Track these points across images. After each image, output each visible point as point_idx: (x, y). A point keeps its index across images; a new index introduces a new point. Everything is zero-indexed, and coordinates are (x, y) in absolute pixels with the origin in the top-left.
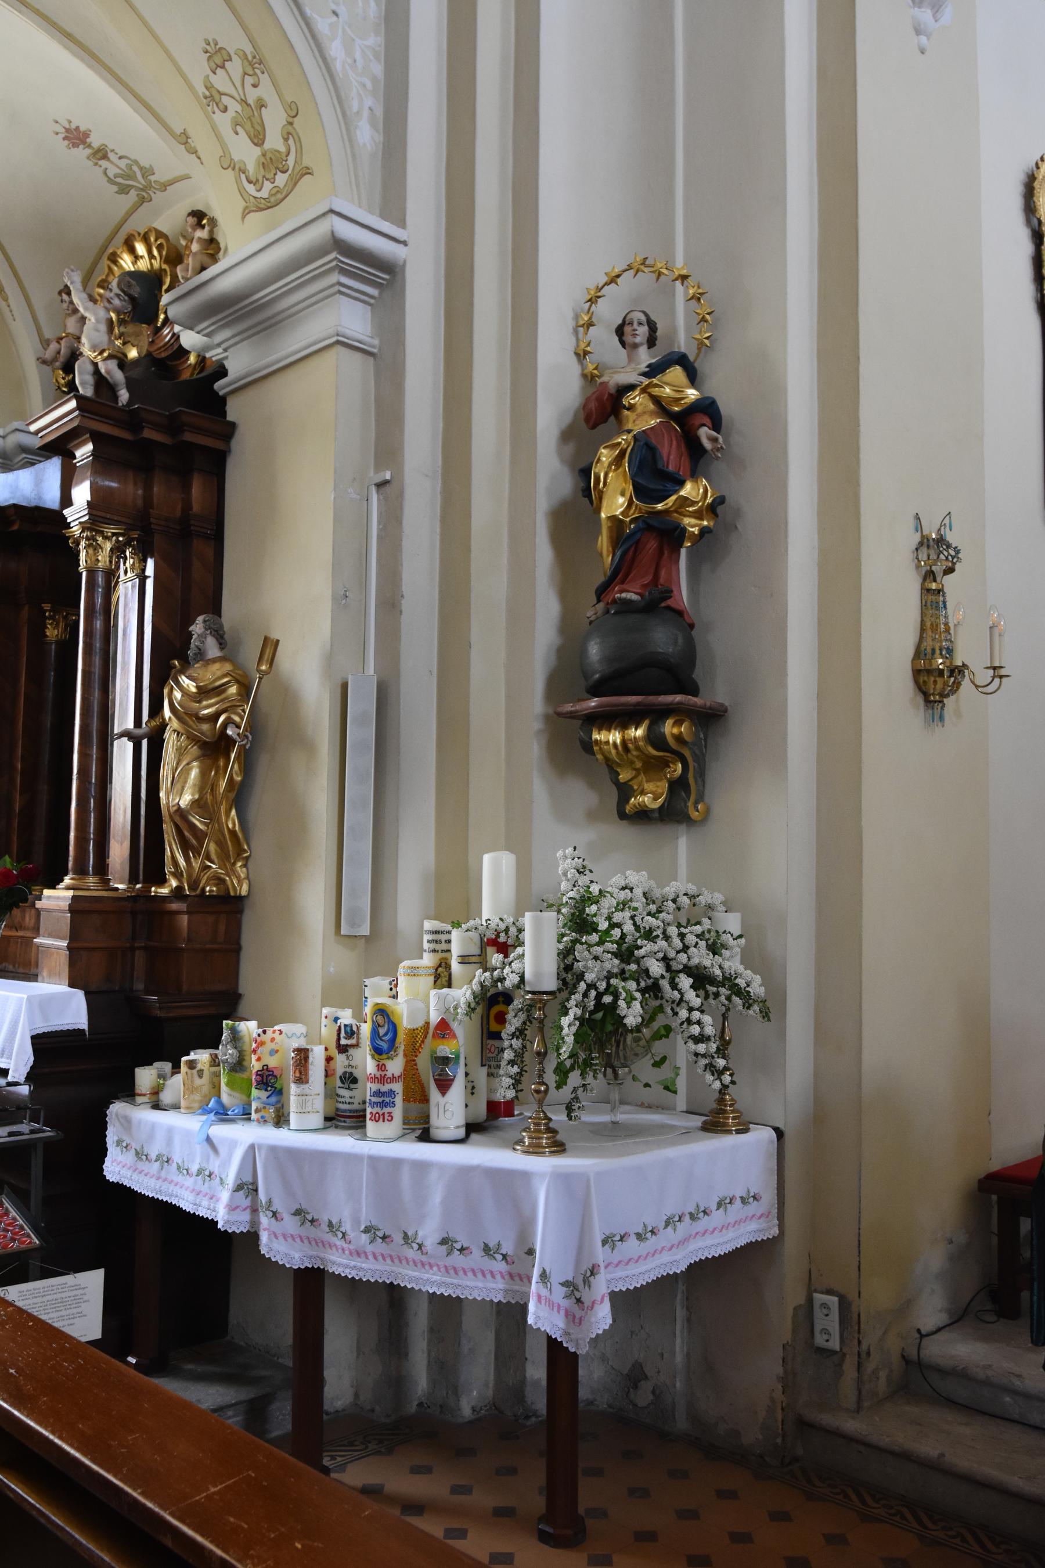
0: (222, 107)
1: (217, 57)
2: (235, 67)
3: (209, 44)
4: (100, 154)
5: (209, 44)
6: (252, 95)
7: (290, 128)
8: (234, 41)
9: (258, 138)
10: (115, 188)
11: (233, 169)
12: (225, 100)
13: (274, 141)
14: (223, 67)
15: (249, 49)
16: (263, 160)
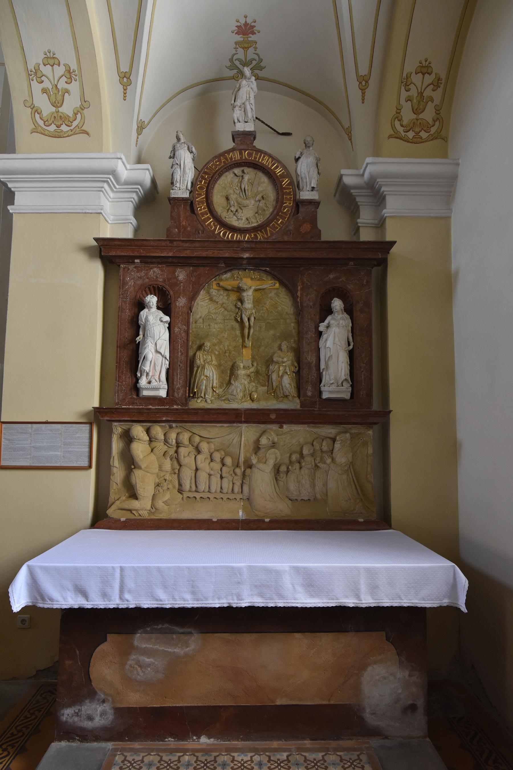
0: (407, 88)
1: (424, 69)
2: (429, 79)
3: (426, 61)
4: (246, 45)
5: (426, 61)
6: (428, 93)
7: (80, 110)
8: (67, 56)
9: (57, 104)
10: (229, 64)
11: (32, 109)
12: (43, 78)
13: (68, 108)
14: (424, 74)
15: (74, 66)
16: (55, 115)
